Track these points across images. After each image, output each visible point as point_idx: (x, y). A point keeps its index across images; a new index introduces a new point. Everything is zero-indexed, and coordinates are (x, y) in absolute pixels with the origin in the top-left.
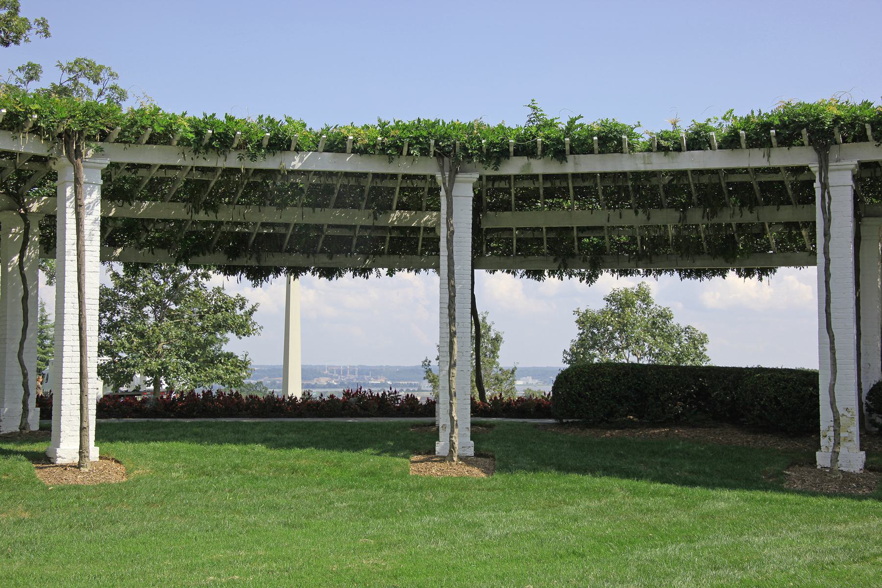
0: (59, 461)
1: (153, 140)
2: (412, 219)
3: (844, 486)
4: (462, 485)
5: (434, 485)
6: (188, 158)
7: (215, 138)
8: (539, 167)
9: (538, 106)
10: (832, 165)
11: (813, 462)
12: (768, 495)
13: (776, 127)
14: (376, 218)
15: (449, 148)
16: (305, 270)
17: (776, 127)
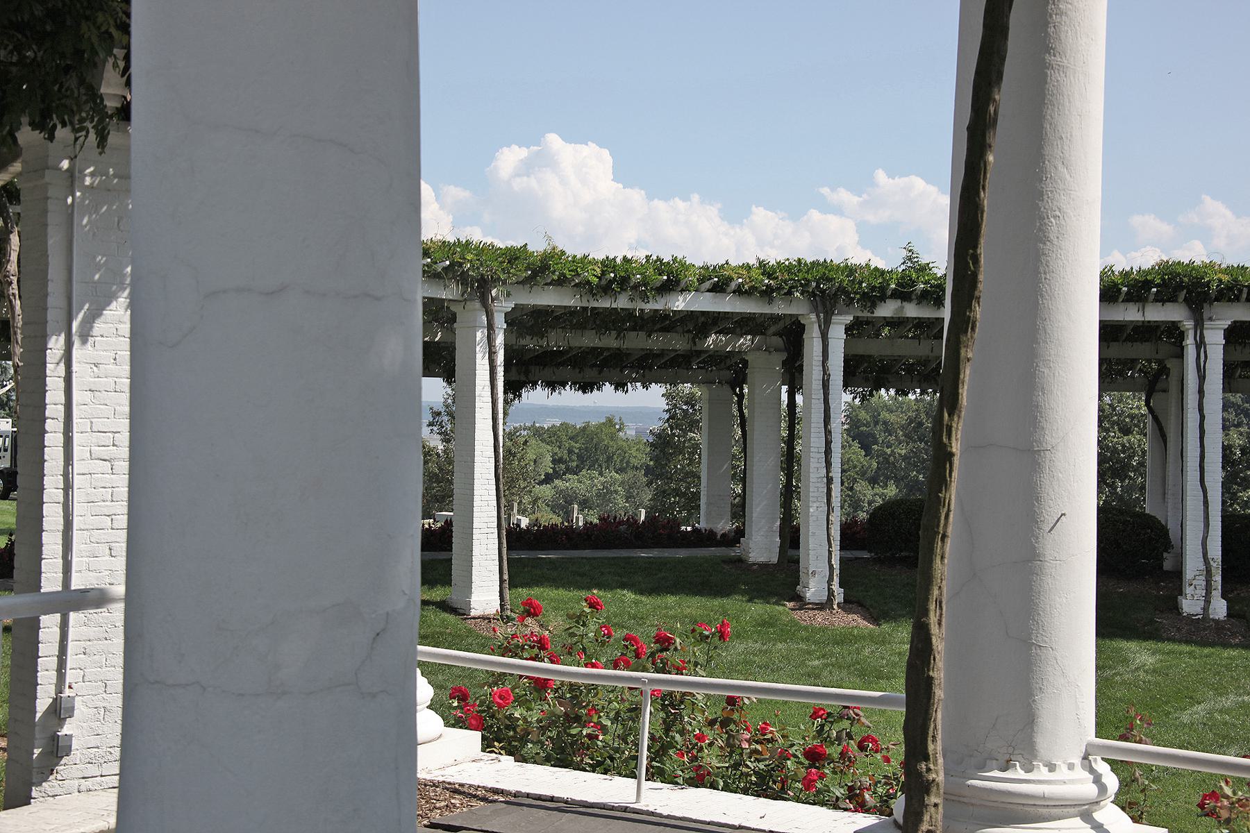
0: (473, 613)
1: (561, 282)
2: (727, 345)
3: (1201, 632)
4: (845, 638)
5: (811, 635)
6: (585, 300)
7: (616, 276)
8: (912, 311)
9: (915, 249)
10: (1207, 324)
11: (1176, 608)
12: (1176, 647)
13: (1157, 286)
14: (695, 343)
15: (827, 287)
16: (563, 385)
17: (1157, 286)
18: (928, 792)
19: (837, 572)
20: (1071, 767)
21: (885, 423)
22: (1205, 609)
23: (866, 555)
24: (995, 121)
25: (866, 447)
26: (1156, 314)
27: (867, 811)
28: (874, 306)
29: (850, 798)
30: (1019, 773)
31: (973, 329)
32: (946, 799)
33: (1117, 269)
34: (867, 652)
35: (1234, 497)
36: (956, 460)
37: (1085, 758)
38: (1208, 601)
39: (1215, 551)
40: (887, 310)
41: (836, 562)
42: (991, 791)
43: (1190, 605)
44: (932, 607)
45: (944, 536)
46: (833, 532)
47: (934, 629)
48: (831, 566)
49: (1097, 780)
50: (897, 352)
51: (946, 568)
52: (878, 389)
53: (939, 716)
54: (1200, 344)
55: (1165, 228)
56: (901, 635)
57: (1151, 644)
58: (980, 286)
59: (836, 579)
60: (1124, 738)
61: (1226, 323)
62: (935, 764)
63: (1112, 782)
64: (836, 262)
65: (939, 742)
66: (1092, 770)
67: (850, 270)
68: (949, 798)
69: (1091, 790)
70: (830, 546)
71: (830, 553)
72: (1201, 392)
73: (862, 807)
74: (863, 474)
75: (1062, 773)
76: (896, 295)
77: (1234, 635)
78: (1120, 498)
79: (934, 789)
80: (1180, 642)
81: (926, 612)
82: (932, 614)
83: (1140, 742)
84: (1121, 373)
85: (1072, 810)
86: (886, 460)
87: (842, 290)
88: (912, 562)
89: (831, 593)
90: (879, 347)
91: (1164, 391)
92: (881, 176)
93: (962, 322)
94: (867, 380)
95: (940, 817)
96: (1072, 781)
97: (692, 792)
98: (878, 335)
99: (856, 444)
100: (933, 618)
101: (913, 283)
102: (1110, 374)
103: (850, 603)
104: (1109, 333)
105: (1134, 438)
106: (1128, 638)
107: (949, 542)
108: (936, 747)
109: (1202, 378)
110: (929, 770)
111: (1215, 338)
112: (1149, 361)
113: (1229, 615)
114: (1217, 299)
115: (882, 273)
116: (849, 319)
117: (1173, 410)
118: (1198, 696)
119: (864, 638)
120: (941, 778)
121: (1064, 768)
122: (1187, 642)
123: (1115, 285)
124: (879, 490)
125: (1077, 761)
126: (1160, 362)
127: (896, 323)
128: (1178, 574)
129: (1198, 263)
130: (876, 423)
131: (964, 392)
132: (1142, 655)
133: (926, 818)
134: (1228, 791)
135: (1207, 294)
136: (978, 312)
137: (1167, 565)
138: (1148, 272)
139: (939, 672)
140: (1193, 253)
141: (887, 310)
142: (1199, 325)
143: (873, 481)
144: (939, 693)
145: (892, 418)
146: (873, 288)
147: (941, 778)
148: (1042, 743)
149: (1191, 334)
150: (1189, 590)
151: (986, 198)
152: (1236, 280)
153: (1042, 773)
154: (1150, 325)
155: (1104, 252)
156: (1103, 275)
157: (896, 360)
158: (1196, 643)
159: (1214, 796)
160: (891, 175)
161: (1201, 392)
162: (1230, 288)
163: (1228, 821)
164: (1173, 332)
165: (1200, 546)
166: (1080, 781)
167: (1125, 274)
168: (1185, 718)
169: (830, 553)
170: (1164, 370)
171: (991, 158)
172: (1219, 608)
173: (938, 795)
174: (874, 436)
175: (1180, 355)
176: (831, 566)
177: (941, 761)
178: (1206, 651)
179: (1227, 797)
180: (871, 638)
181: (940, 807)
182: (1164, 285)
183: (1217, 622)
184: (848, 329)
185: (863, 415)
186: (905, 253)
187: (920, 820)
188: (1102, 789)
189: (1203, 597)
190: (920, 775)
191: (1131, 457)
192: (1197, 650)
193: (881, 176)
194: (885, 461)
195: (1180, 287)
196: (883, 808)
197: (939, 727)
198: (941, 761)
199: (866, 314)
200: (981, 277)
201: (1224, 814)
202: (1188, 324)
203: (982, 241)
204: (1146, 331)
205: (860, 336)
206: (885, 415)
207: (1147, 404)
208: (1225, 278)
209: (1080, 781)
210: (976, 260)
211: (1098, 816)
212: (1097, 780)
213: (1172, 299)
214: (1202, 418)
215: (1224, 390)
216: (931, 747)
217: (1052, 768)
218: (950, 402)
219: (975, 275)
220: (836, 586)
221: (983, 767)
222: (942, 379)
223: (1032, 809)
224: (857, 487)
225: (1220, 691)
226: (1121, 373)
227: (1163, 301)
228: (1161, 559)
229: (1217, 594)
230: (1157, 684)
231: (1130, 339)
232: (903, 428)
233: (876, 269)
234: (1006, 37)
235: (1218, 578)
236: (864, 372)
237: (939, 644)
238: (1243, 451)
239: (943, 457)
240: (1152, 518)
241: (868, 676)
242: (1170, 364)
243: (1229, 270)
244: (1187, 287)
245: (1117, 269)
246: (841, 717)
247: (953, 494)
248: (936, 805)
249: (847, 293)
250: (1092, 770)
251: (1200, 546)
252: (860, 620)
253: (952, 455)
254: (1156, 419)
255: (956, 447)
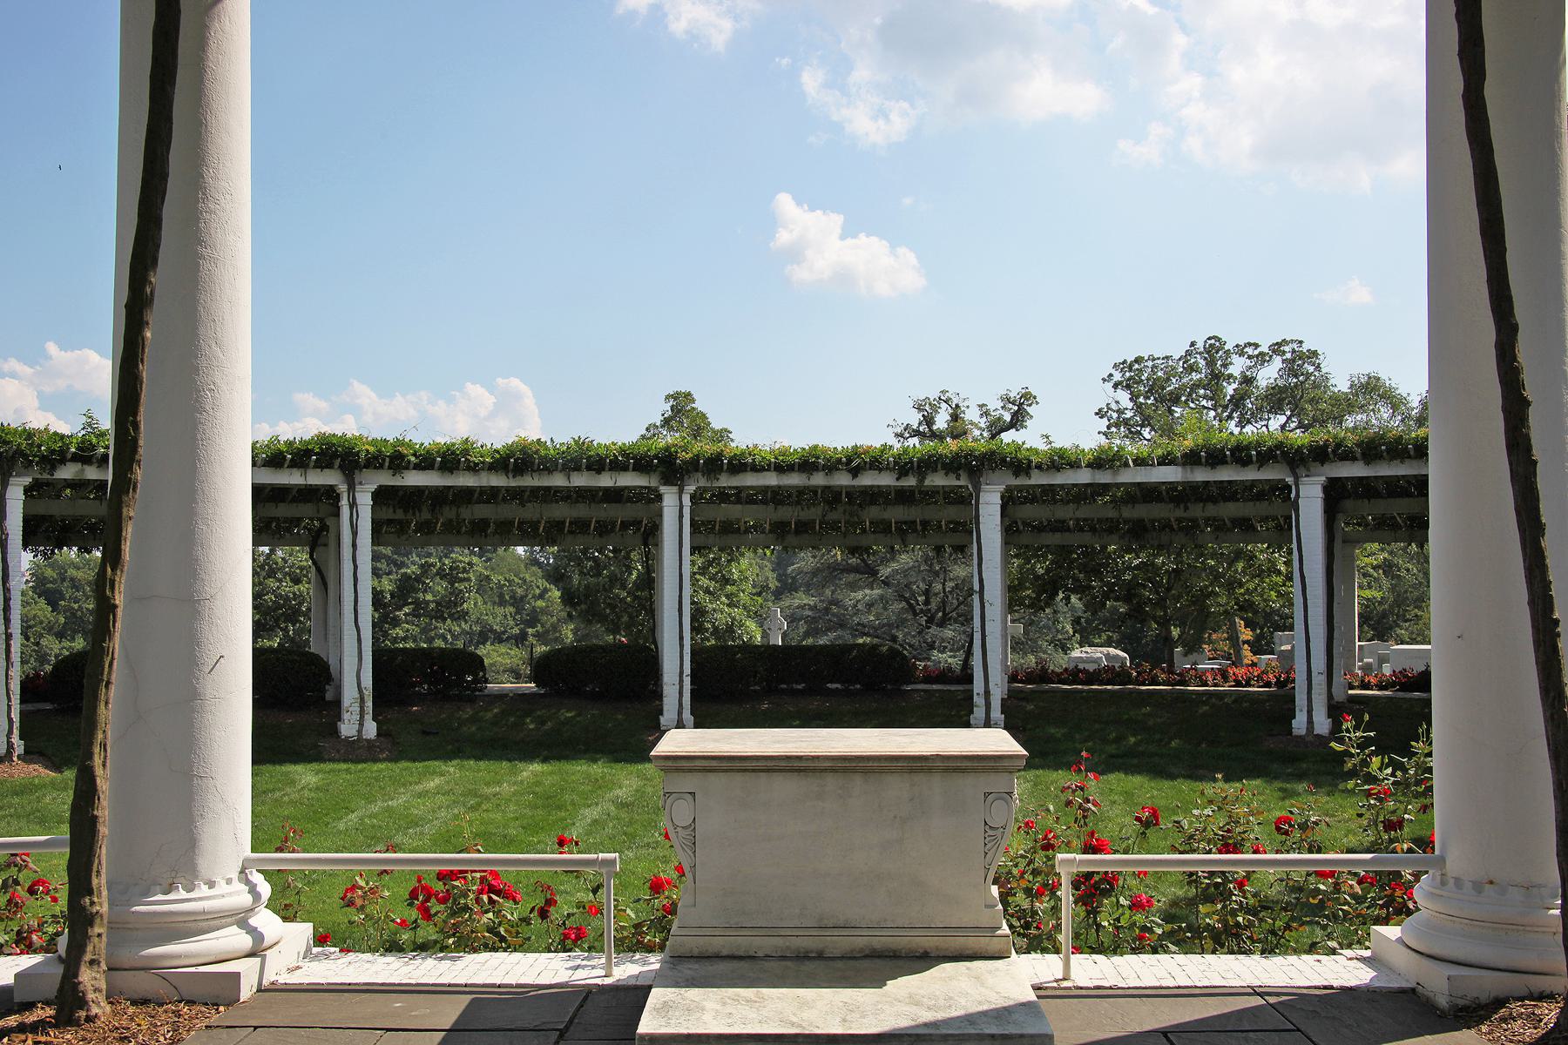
3: (357, 751)
10: (358, 488)
11: (335, 732)
18: (91, 924)
19: (16, 725)
20: (229, 881)
21: (72, 579)
22: (360, 731)
23: (48, 706)
24: (152, 300)
25: (53, 604)
26: (317, 478)
27: (35, 952)
28: (53, 468)
29: (17, 943)
30: (183, 894)
31: (134, 490)
32: (110, 928)
33: (283, 439)
34: (48, 799)
35: (386, 634)
36: (119, 612)
37: (242, 872)
38: (361, 725)
39: (367, 680)
40: (67, 472)
41: (16, 716)
42: (155, 913)
43: (347, 729)
44: (96, 750)
45: (108, 683)
46: (12, 686)
47: (99, 771)
48: (10, 721)
49: (253, 890)
50: (79, 512)
51: (111, 713)
52: (60, 548)
53: (104, 852)
54: (353, 505)
55: (323, 405)
56: (70, 774)
57: (315, 766)
58: (141, 451)
59: (16, 732)
60: (280, 850)
61: (373, 487)
62: (99, 896)
63: (265, 889)
64: (13, 426)
65: (103, 876)
66: (248, 882)
67: (29, 435)
68: (113, 927)
69: (247, 899)
70: (9, 699)
71: (9, 707)
72: (354, 546)
73: (30, 949)
74: (50, 629)
75: (222, 888)
76: (76, 458)
77: (382, 751)
78: (292, 640)
79: (98, 921)
80: (339, 761)
81: (90, 756)
82: (96, 758)
83: (293, 851)
84: (289, 530)
85: (229, 920)
86: (74, 615)
87: (20, 453)
88: (77, 710)
89: (10, 746)
90: (57, 508)
91: (326, 545)
92: (52, 348)
93: (124, 482)
94: (48, 538)
95: (103, 945)
96: (230, 894)
97: (470, 958)
98: (58, 497)
99: (42, 602)
100: (97, 761)
101: (93, 447)
102: (263, 529)
103: (30, 755)
104: (262, 495)
105: (303, 587)
106: (295, 762)
107: (113, 688)
108: (100, 882)
109: (355, 533)
110: (92, 903)
111: (365, 500)
112: (312, 519)
113: (379, 735)
114: (366, 466)
115: (62, 437)
116: (28, 480)
117: (332, 562)
118: (353, 806)
119: (44, 786)
120: (105, 909)
121: (223, 883)
122: (345, 761)
123: (281, 453)
124: (67, 644)
125: (235, 876)
126: (321, 520)
127: (78, 485)
128: (337, 703)
129: (349, 435)
130: (63, 580)
131: (127, 548)
132: (306, 775)
133: (90, 948)
134: (362, 883)
135: (357, 462)
136: (139, 474)
137: (329, 696)
138: (309, 443)
139: (104, 810)
140: (345, 426)
141: (67, 472)
142: (351, 488)
143: (60, 636)
144: (103, 830)
145: (79, 574)
146: (53, 452)
147: (105, 909)
148: (203, 864)
149: (345, 496)
150: (346, 716)
151: (145, 371)
152: (380, 451)
153: (203, 890)
154: (299, 490)
155: (257, 419)
156: (254, 444)
157: (77, 520)
158: (353, 761)
159: (354, 887)
160: (63, 347)
161: (354, 546)
162: (375, 458)
163: (363, 907)
164: (331, 494)
165: (355, 676)
166: (238, 893)
167: (290, 443)
168: (342, 826)
169: (9, 707)
170: (324, 528)
171: (148, 334)
172: (371, 729)
173: (101, 925)
174: (61, 593)
175: (337, 514)
176: (10, 721)
177: (105, 893)
178: (360, 766)
179: (361, 888)
180: (53, 783)
181: (104, 938)
182: (322, 453)
183: (368, 741)
184: (27, 490)
185: (49, 573)
186: (84, 419)
187: (84, 952)
188: (256, 895)
189: (357, 719)
190: (84, 908)
191: (300, 604)
192: (352, 767)
193: (52, 348)
194: (72, 616)
195: (335, 455)
196: (50, 947)
197: (104, 862)
198: (105, 893)
199: (46, 476)
200: (141, 442)
201: (359, 902)
202: (343, 488)
203: (142, 409)
204: (308, 494)
205: (40, 497)
206: (72, 572)
207: (311, 557)
208: (372, 449)
209: (238, 893)
210: (136, 426)
211: (253, 922)
212: (253, 890)
213: (330, 466)
214: (356, 567)
215: (373, 543)
216: (95, 881)
217: (211, 884)
218: (113, 557)
219: (135, 440)
220: (15, 739)
221: (147, 893)
222: (104, 532)
223: (192, 925)
224: (44, 642)
225: (370, 800)
226: (289, 530)
227: (322, 468)
228: (324, 691)
229: (369, 717)
230: (319, 799)
231: (294, 500)
232: (89, 583)
233: (56, 433)
234: (160, 228)
235: (369, 704)
236: (46, 530)
237: (103, 784)
238: (392, 596)
239: (106, 609)
240: (317, 657)
241: (42, 821)
242: (330, 522)
243: (374, 442)
244: (336, 454)
245: (283, 439)
246: (8, 866)
247: (117, 643)
248: (99, 935)
249: (25, 456)
250: (248, 882)
251: (355, 676)
252: (41, 770)
253: (115, 606)
254: (319, 570)
255: (119, 599)
